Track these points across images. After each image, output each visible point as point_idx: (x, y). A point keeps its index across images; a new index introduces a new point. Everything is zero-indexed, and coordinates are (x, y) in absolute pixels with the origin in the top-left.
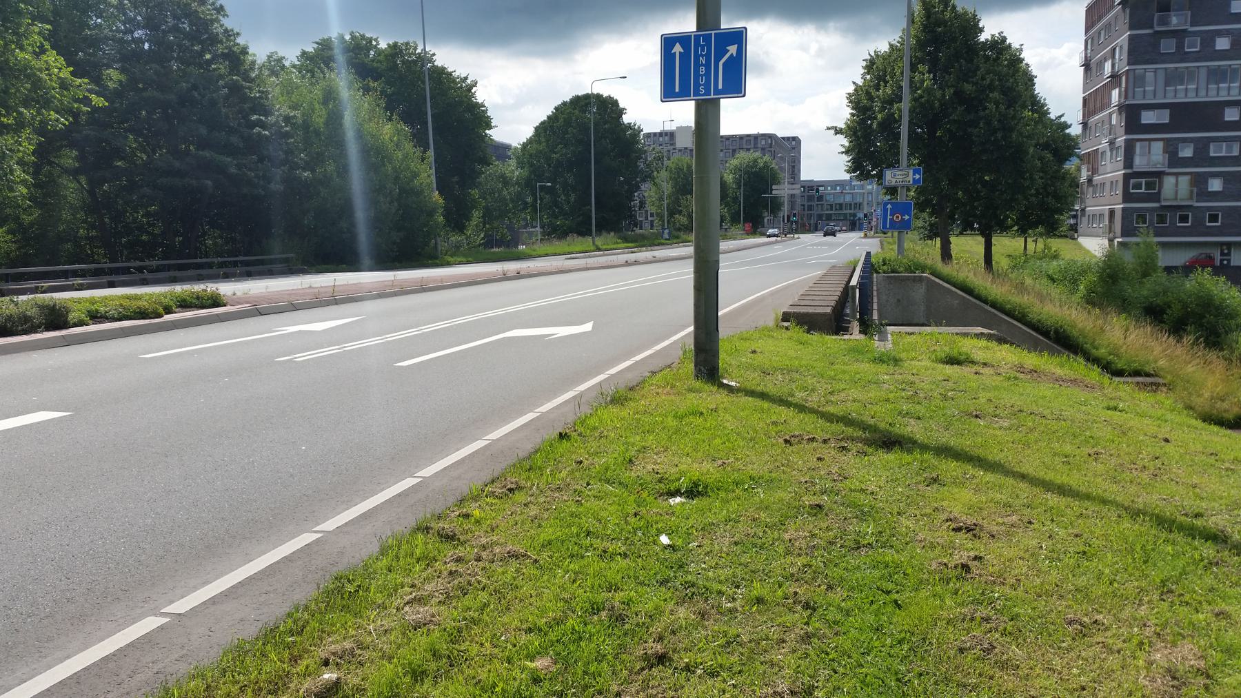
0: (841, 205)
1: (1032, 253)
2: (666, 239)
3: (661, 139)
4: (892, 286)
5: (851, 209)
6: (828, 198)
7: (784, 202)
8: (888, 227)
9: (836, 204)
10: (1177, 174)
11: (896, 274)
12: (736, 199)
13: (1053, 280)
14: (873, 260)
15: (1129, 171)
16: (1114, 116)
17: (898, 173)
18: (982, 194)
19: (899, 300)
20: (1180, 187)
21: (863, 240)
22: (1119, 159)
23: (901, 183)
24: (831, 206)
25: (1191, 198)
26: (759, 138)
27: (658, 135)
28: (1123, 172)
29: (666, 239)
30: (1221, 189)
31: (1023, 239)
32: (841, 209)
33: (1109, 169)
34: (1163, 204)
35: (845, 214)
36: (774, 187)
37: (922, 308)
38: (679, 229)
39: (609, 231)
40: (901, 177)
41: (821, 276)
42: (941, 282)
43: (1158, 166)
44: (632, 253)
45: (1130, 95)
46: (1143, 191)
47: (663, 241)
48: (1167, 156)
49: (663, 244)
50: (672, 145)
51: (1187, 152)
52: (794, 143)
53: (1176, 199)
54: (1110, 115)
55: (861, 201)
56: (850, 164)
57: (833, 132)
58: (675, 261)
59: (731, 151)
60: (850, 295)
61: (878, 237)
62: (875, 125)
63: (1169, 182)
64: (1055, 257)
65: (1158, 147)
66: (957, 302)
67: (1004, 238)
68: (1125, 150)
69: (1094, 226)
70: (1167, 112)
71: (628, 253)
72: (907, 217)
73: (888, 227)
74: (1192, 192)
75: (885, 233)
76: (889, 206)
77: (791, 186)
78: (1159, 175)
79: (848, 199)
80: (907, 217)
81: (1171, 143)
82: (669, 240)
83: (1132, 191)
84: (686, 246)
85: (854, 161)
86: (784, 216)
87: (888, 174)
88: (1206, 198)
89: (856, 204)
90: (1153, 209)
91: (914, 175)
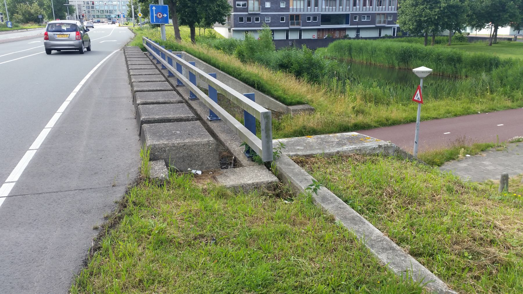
0: (103, 11)
5: (108, 13)
6: (96, 8)
7: (76, 8)
8: (155, 21)
9: (101, 10)
12: (49, 7)
18: (189, 5)
24: (98, 11)
25: (259, 10)
30: (270, 7)
38: (18, 22)
42: (193, 57)
46: (241, 7)
49: (7, 31)
53: (254, 11)
58: (5, 44)
73: (155, 21)
74: (259, 8)
79: (106, 8)
82: (12, 28)
83: (237, 7)
84: (22, 32)
86: (77, 16)
88: (265, 11)
89: (110, 10)
90: (246, 15)
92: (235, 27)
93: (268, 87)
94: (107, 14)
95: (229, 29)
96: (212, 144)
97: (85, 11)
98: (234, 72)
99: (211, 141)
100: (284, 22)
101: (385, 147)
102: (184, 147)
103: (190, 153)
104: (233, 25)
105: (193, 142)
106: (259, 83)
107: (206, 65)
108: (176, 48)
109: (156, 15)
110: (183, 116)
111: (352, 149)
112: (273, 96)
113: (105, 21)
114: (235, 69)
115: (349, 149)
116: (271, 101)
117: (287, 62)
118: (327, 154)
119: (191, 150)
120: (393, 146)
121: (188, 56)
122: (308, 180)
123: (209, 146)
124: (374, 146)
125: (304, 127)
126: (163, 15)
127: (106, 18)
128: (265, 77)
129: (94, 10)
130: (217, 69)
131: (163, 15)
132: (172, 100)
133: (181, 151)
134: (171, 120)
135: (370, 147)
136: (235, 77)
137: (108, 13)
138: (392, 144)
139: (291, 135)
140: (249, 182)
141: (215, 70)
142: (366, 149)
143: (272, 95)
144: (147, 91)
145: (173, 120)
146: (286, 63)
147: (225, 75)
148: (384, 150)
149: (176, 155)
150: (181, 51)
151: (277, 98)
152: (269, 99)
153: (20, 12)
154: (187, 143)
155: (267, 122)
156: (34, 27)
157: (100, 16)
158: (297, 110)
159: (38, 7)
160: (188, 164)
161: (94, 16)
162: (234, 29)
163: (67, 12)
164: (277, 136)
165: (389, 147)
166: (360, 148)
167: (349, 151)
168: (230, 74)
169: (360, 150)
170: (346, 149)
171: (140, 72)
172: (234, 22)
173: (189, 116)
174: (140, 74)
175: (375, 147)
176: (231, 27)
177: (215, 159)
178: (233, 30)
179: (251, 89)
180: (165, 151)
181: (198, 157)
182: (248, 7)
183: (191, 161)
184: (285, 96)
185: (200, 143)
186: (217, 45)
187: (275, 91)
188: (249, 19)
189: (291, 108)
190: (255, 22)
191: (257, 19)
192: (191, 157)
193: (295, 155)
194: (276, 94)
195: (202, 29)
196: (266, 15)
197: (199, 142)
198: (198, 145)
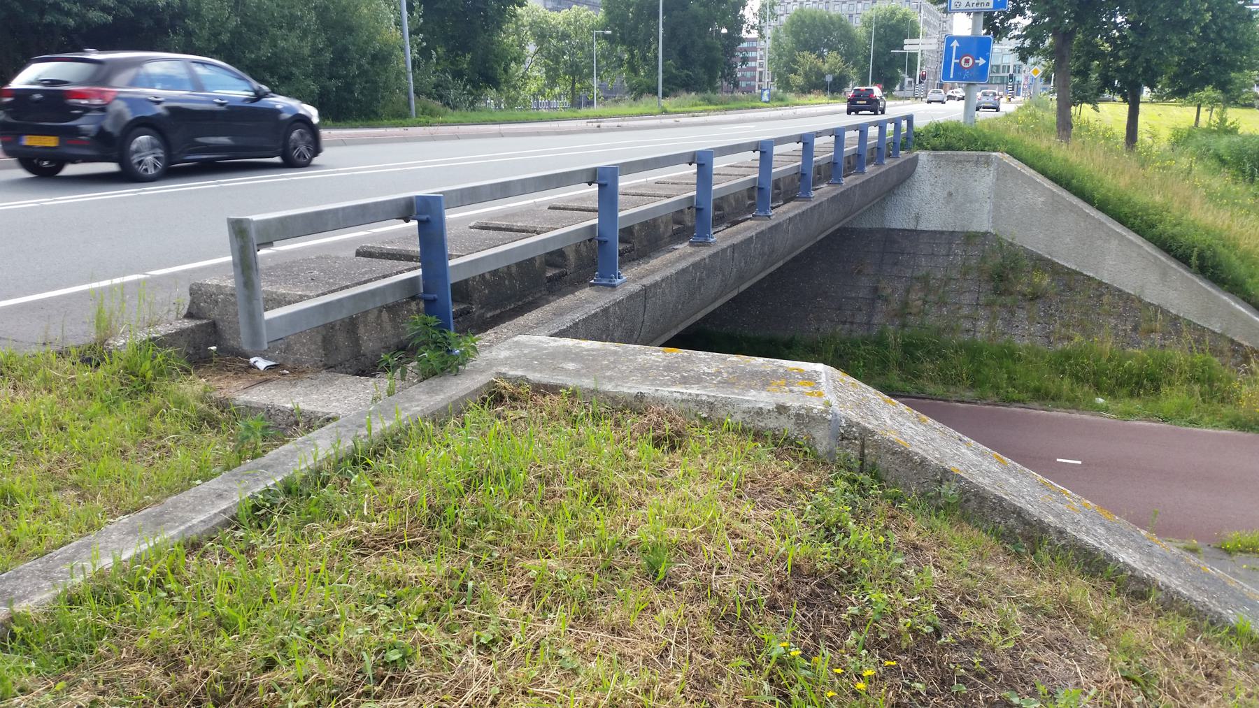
0: (998, 67)
2: (766, 102)
4: (940, 172)
8: (951, 77)
13: (1223, 162)
19: (950, 194)
23: (975, 7)
29: (766, 102)
31: (1196, 108)
32: (998, 71)
37: (988, 207)
39: (688, 91)
47: (760, 104)
67: (1172, 107)
73: (951, 77)
80: (982, 61)
93: (1241, 270)
98: (1136, 217)
101: (798, 416)
106: (1208, 253)
107: (1051, 191)
109: (958, 61)
111: (685, 397)
115: (675, 395)
122: (334, 419)
124: (761, 405)
126: (977, 61)
131: (977, 61)
134: (413, 257)
135: (746, 405)
136: (1137, 232)
141: (1076, 206)
143: (1250, 296)
147: (1101, 223)
148: (796, 423)
152: (1229, 305)
153: (801, 71)
163: (903, 68)
164: (1206, 419)
166: (712, 400)
168: (1122, 221)
169: (711, 406)
170: (666, 394)
175: (761, 409)
177: (315, 343)
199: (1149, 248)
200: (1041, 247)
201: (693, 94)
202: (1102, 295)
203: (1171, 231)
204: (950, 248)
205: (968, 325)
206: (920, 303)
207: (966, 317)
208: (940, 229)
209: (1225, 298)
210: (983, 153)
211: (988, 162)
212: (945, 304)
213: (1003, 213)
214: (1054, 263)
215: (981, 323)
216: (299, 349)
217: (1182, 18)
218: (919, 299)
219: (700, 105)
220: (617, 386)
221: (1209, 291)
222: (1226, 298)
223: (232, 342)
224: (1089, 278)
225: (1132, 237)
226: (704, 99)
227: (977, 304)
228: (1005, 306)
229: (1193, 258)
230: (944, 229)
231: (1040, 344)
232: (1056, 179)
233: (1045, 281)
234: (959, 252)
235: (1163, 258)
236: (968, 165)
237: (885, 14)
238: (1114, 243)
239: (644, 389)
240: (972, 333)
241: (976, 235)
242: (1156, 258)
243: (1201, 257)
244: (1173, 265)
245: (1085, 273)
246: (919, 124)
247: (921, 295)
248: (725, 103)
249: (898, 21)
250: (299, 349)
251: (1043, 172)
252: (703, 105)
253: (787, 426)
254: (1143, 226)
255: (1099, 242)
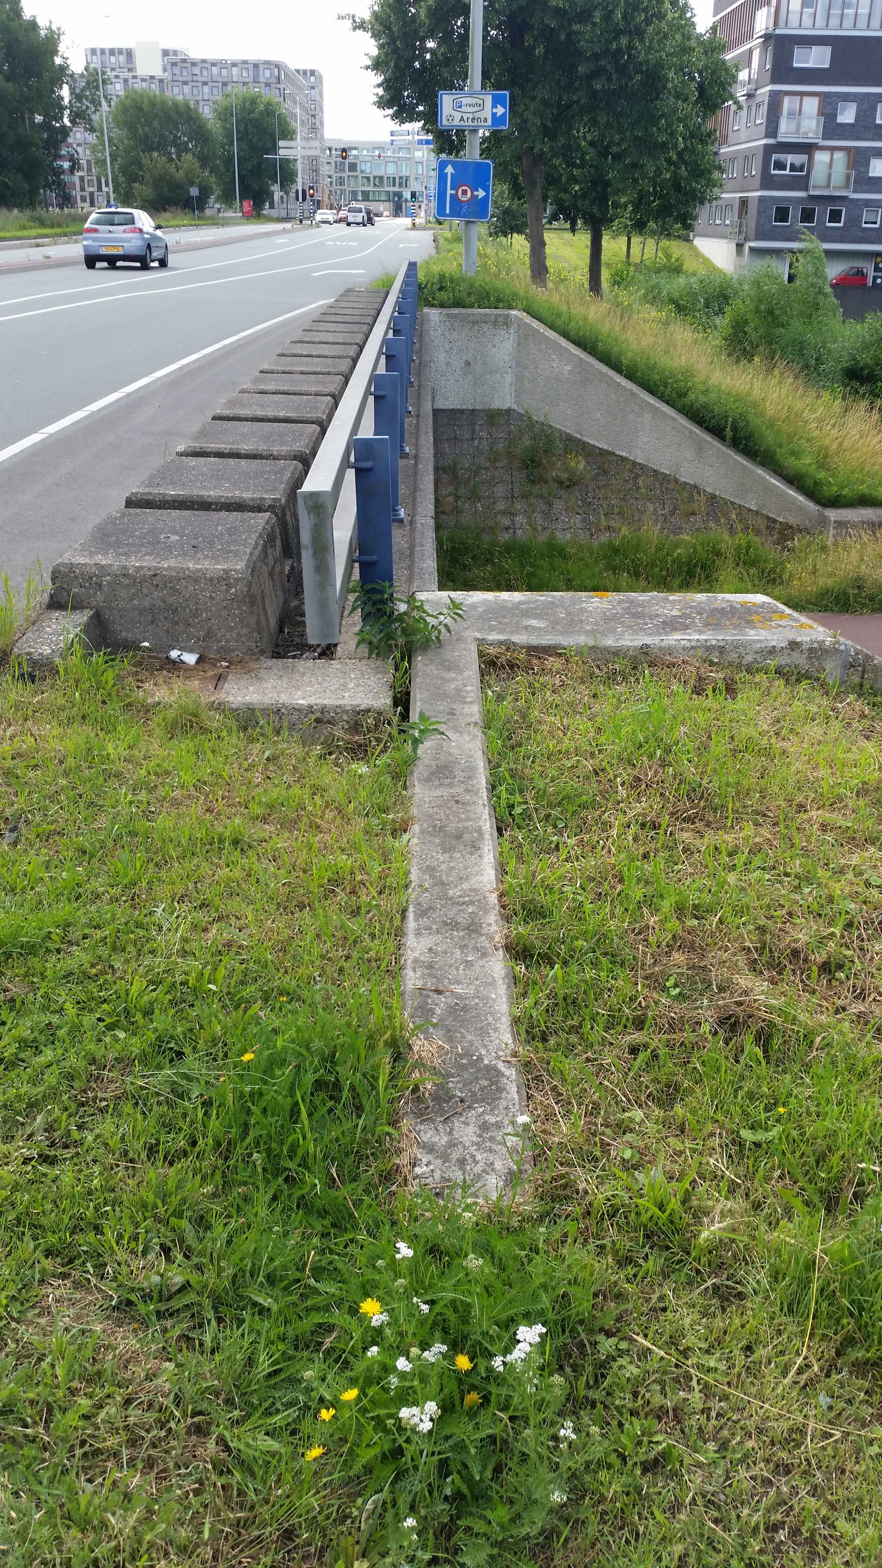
1: (638, 260)
3: (113, 59)
4: (455, 335)
5: (394, 185)
6: (363, 168)
8: (448, 212)
9: (375, 177)
10: (832, 149)
11: (464, 311)
14: (421, 276)
15: (771, 141)
16: (756, 54)
17: (465, 101)
19: (468, 364)
20: (834, 169)
21: (411, 233)
22: (758, 122)
24: (368, 179)
26: (261, 67)
27: (107, 52)
28: (764, 142)
33: (743, 136)
34: (812, 193)
35: (388, 193)
36: (281, 143)
37: (509, 379)
40: (471, 109)
41: (298, 335)
43: (810, 135)
44: (38, 246)
45: (782, 22)
46: (787, 172)
48: (822, 119)
50: (130, 70)
51: (847, 116)
52: (313, 79)
54: (750, 51)
55: (408, 174)
56: (381, 91)
57: (348, 23)
59: (220, 85)
60: (306, 537)
61: (430, 229)
62: (423, 13)
63: (821, 157)
64: (677, 270)
65: (811, 105)
66: (568, 368)
68: (769, 109)
69: (718, 222)
70: (827, 51)
71: (31, 246)
72: (481, 193)
73: (448, 212)
75: (440, 223)
76: (449, 170)
77: (305, 144)
78: (808, 149)
79: (391, 170)
80: (481, 193)
81: (828, 100)
83: (773, 172)
85: (387, 85)
86: (297, 191)
87: (447, 101)
88: (866, 187)
89: (401, 178)
90: (799, 200)
91: (494, 106)
92: (757, 238)
93: (770, 438)
94: (392, 189)
95: (740, 246)
96: (237, 580)
97: (330, 177)
98: (666, 385)
99: (235, 570)
100: (841, 225)
101: (811, 650)
102: (155, 579)
103: (171, 600)
104: (752, 232)
105: (182, 568)
108: (499, 300)
110: (247, 495)
111: (694, 644)
112: (779, 471)
113: (385, 210)
114: (672, 375)
115: (683, 642)
116: (769, 488)
117: (870, 362)
118: (607, 649)
119: (175, 591)
120: (842, 648)
121: (529, 325)
123: (229, 586)
124: (774, 643)
125: (859, 584)
127: (389, 201)
128: (770, 409)
129: (356, 177)
130: (611, 373)
132: (276, 450)
133: (145, 591)
134: (211, 504)
137: (394, 185)
138: (838, 643)
139: (808, 602)
140: (301, 702)
141: (605, 375)
142: (741, 650)
143: (779, 467)
144: (246, 419)
145: (216, 504)
146: (866, 366)
147: (633, 394)
148: (809, 658)
149: (132, 600)
150: (510, 307)
151: (795, 480)
152: (764, 479)
154: (165, 570)
155: (316, 525)
156: (181, 223)
157: (371, 194)
158: (849, 522)
159: (197, 164)
160: (168, 632)
161: (354, 194)
162: (753, 244)
165: (826, 651)
166: (722, 644)
167: (684, 648)
168: (651, 390)
169: (722, 650)
170: (673, 643)
171: (290, 365)
172: (758, 222)
173: (264, 499)
174: (287, 369)
175: (774, 647)
176: (746, 239)
177: (247, 626)
178: (752, 250)
179: (710, 443)
180: (100, 586)
181: (195, 614)
182: (809, 172)
183: (176, 623)
184: (822, 475)
185: (200, 574)
186: (676, 295)
187: (793, 453)
188: (807, 216)
189: (832, 514)
190: (828, 224)
191: (835, 216)
192: (175, 611)
193: (501, 643)
194: (793, 464)
195: (651, 242)
196: (868, 203)
197: (198, 570)
198: (196, 581)
199: (682, 421)
200: (569, 424)
201: (16, 211)
202: (636, 477)
203: (703, 399)
204: (473, 431)
205: (506, 522)
206: (451, 499)
207: (503, 513)
208: (459, 407)
209: (760, 471)
210: (499, 311)
211: (507, 322)
212: (479, 498)
213: (527, 385)
214: (585, 444)
215: (519, 519)
216: (224, 636)
217: (656, 139)
218: (450, 494)
219: (31, 228)
220: (618, 640)
221: (744, 466)
222: (760, 472)
223: (124, 634)
224: (623, 459)
225: (665, 408)
226: (33, 219)
227: (513, 497)
228: (541, 496)
229: (728, 429)
230: (464, 407)
231: (583, 537)
232: (579, 343)
233: (580, 465)
234: (483, 434)
235: (698, 431)
236: (485, 327)
237: (244, 103)
238: (647, 417)
239: (648, 640)
240: (512, 531)
241: (499, 413)
242: (691, 431)
243: (735, 429)
244: (708, 438)
245: (617, 453)
246: (183, 242)
247: (450, 488)
248: (59, 226)
249: (261, 114)
250: (224, 636)
251: (565, 335)
252: (35, 227)
253: (800, 660)
254: (674, 395)
255: (632, 417)
